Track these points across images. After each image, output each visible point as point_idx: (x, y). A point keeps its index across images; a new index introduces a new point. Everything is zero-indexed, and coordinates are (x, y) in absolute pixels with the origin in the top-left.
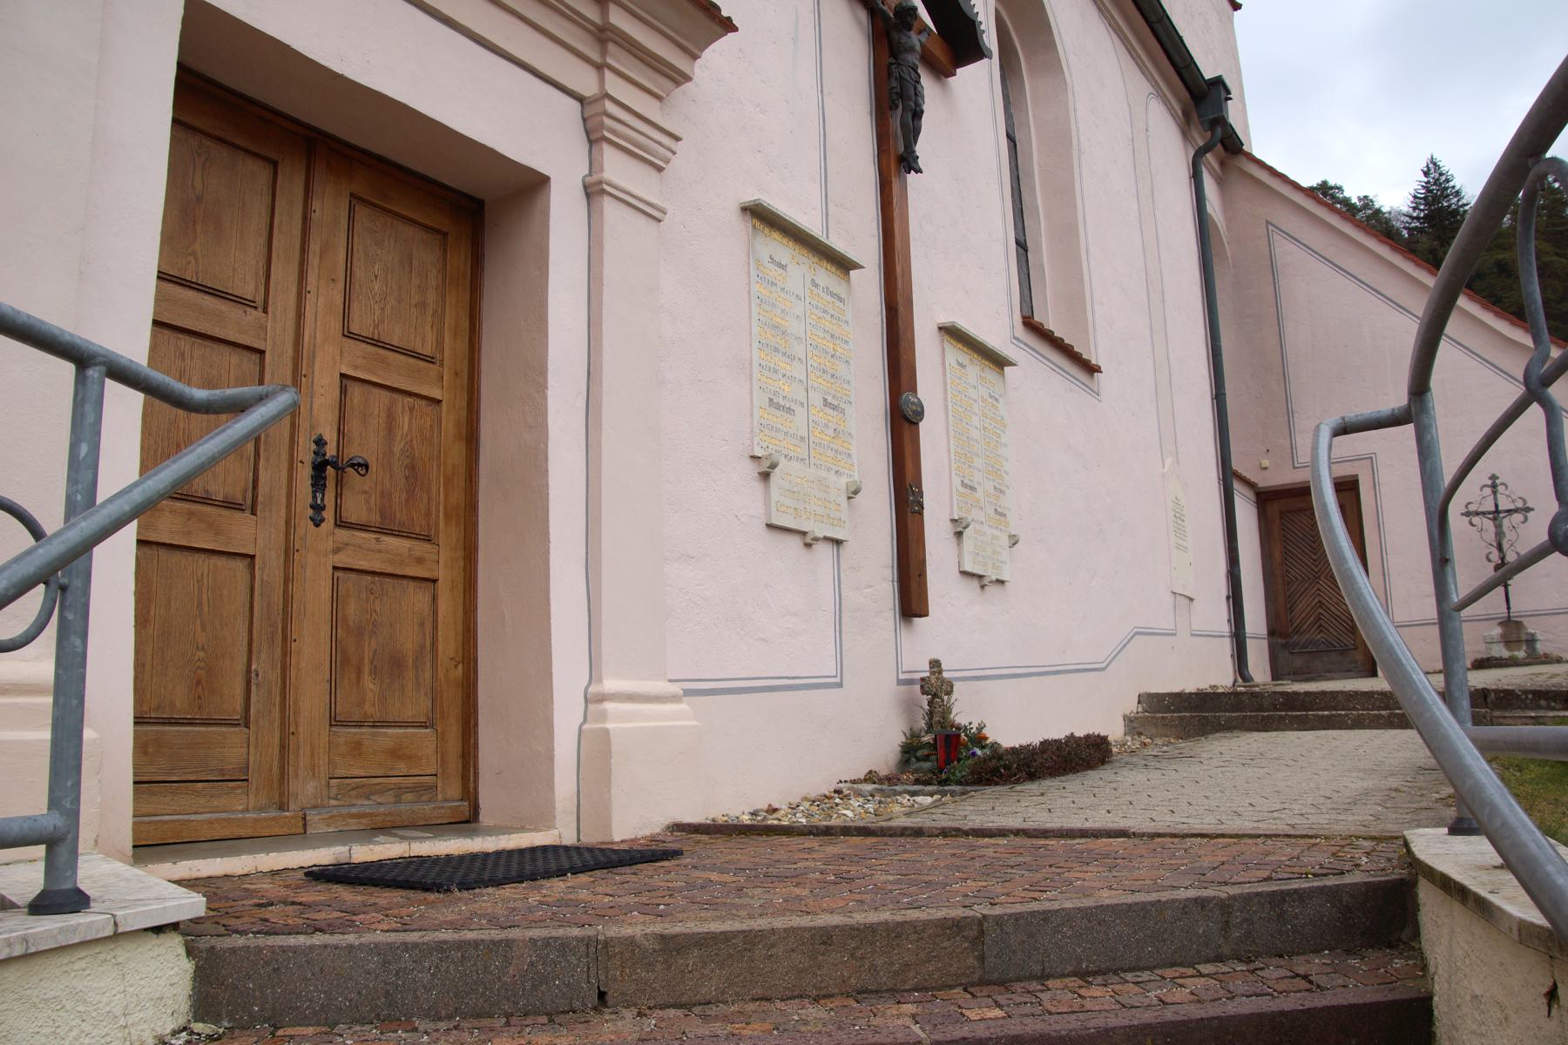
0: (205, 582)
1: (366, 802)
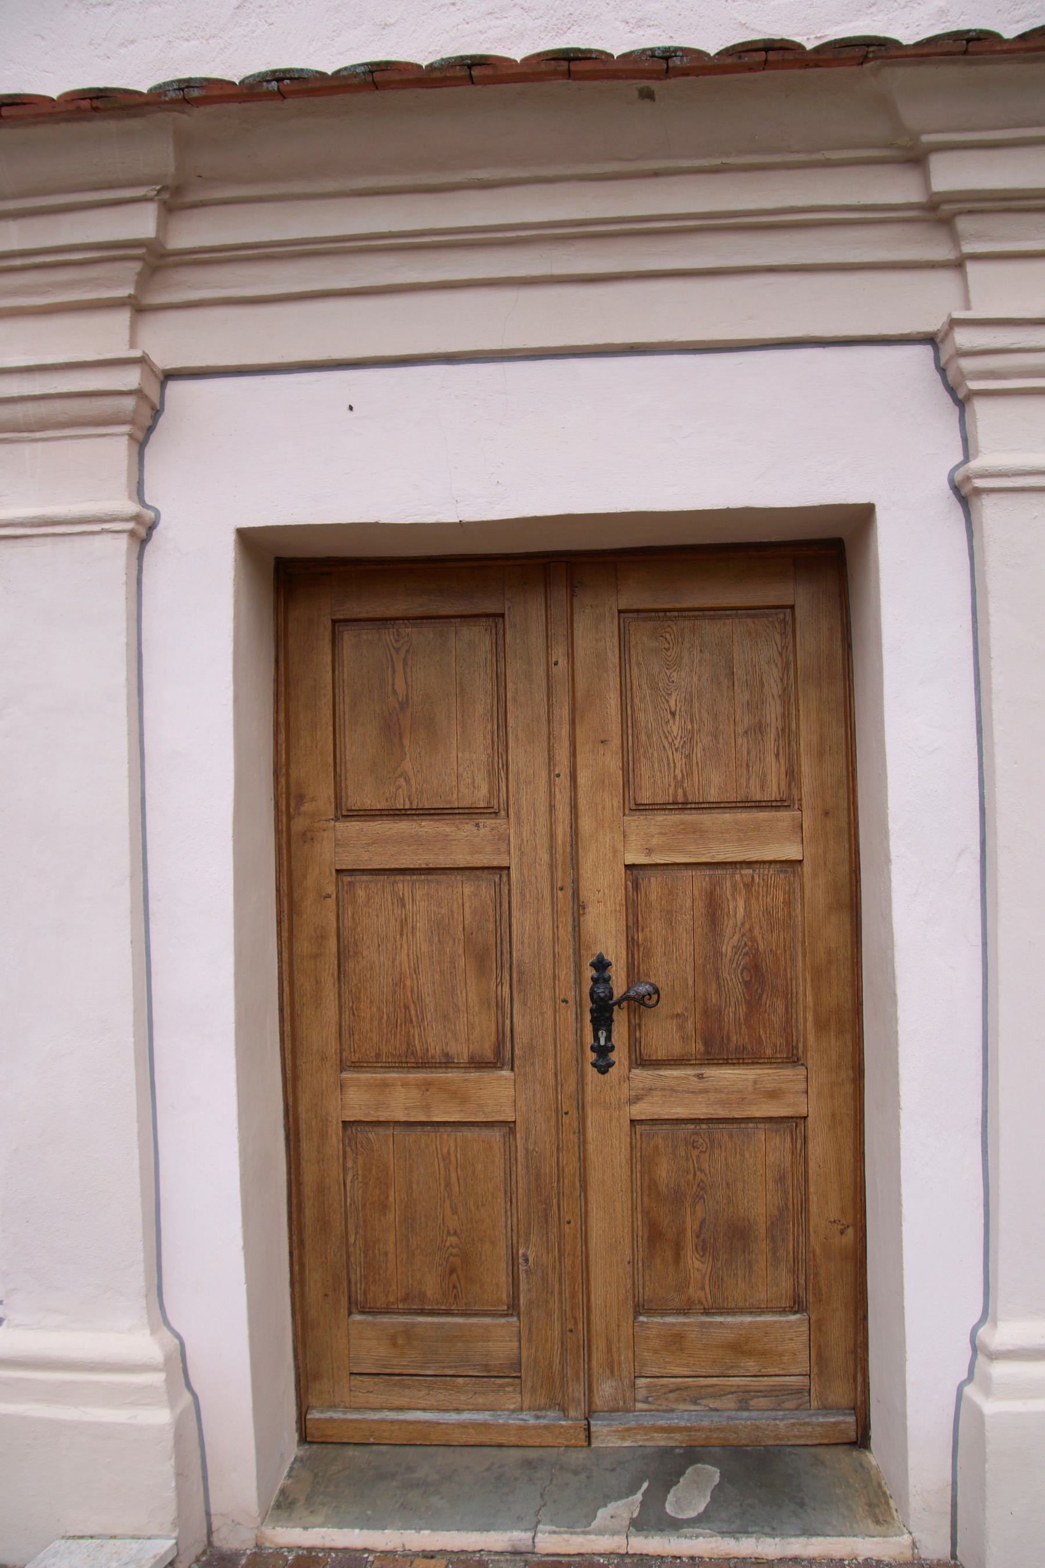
0: (453, 1159)
1: (693, 1408)
